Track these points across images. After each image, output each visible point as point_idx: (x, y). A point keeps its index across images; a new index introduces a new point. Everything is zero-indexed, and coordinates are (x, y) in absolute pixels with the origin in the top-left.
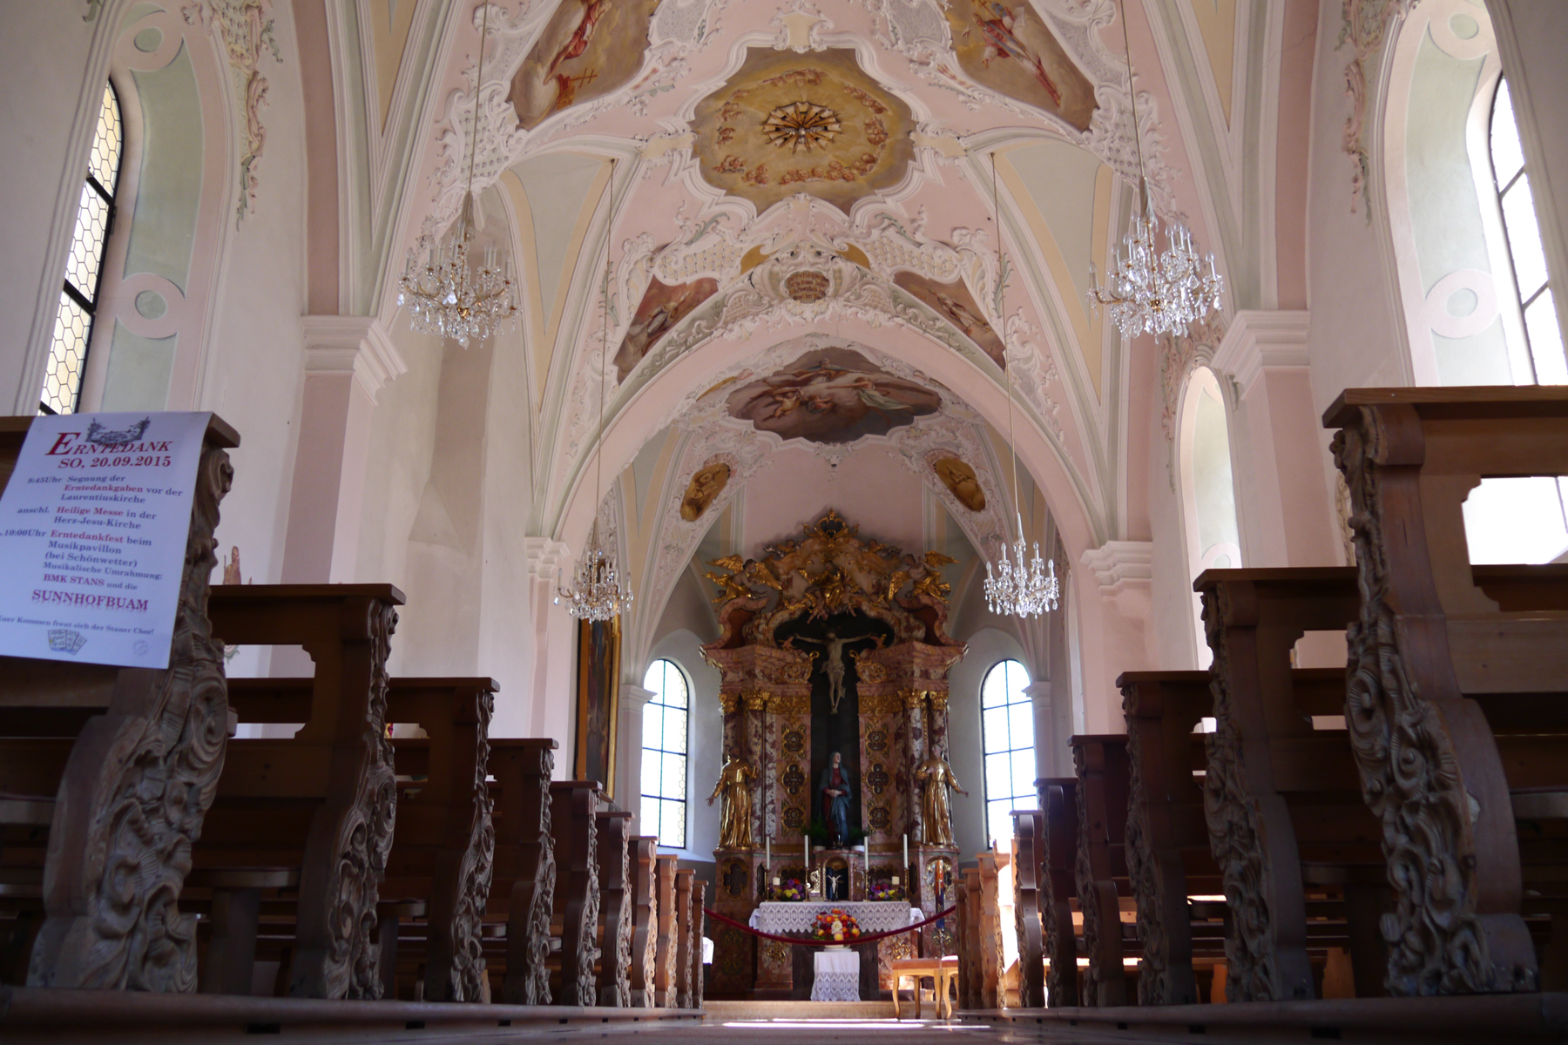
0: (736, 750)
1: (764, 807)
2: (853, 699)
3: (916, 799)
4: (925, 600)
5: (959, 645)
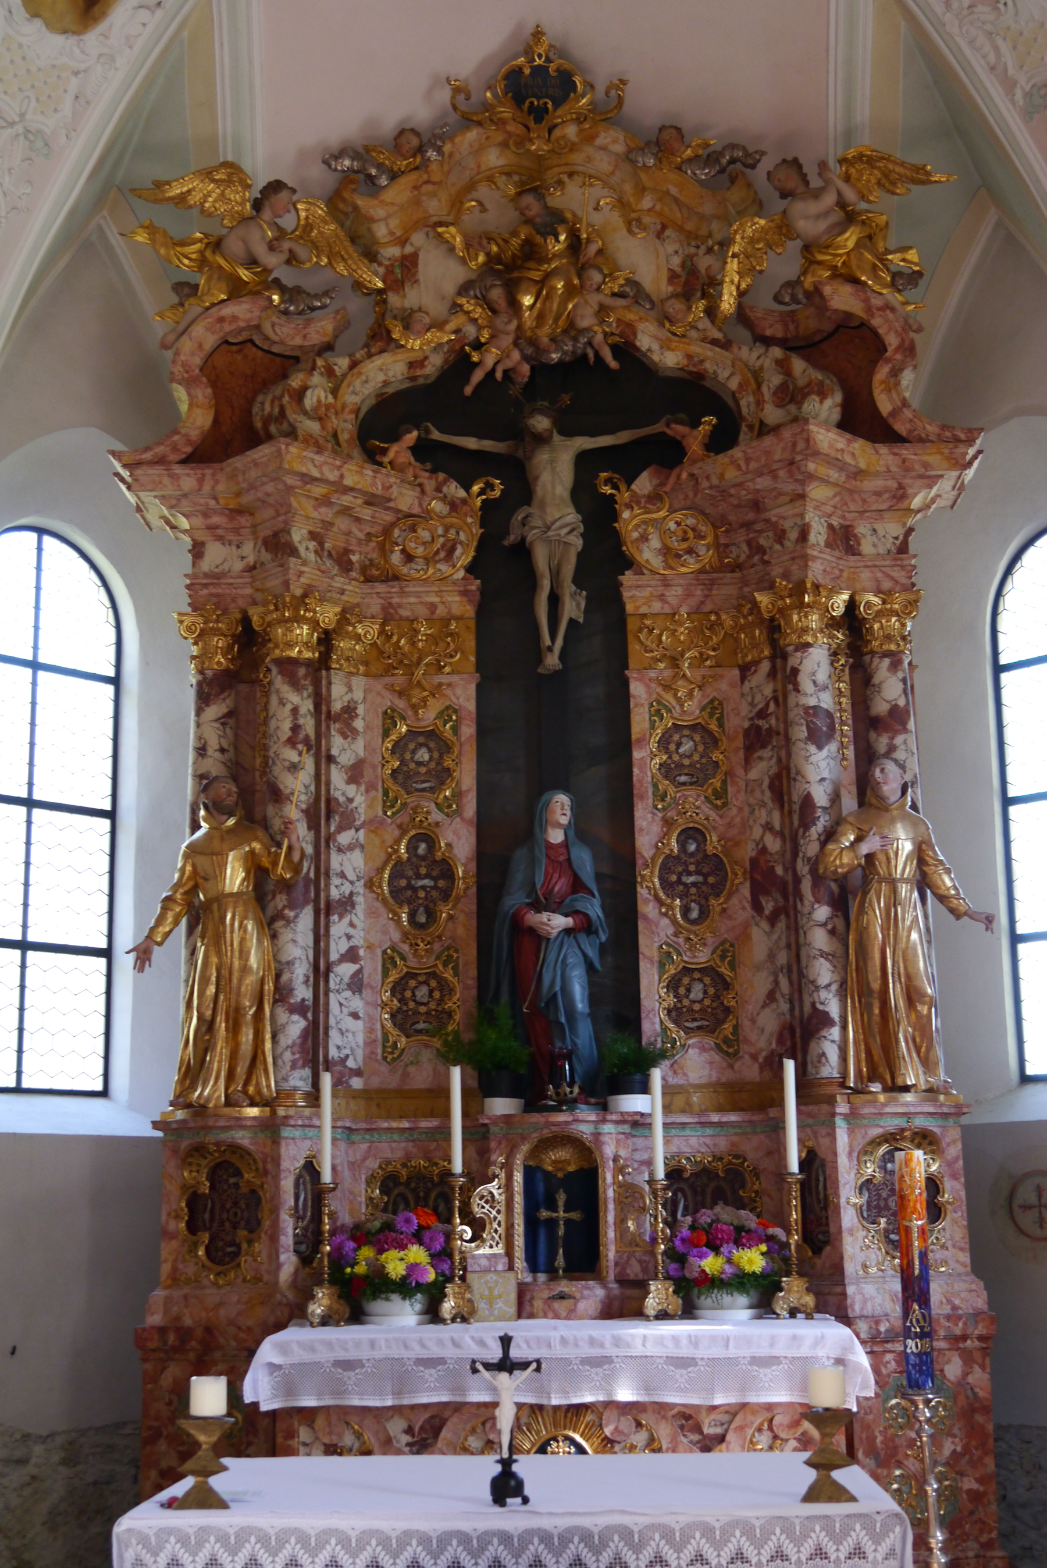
0: (227, 790)
1: (320, 972)
2: (610, 618)
3: (819, 939)
4: (842, 299)
5: (956, 441)
